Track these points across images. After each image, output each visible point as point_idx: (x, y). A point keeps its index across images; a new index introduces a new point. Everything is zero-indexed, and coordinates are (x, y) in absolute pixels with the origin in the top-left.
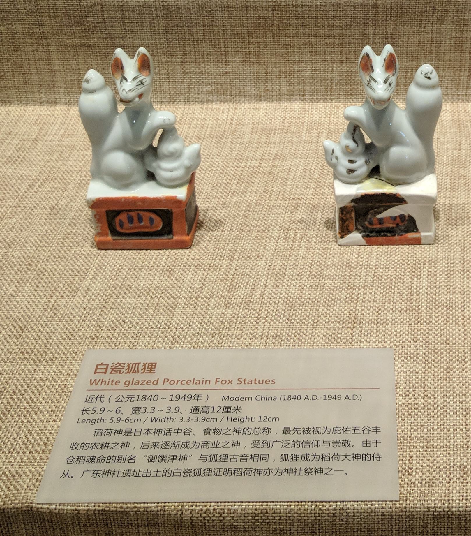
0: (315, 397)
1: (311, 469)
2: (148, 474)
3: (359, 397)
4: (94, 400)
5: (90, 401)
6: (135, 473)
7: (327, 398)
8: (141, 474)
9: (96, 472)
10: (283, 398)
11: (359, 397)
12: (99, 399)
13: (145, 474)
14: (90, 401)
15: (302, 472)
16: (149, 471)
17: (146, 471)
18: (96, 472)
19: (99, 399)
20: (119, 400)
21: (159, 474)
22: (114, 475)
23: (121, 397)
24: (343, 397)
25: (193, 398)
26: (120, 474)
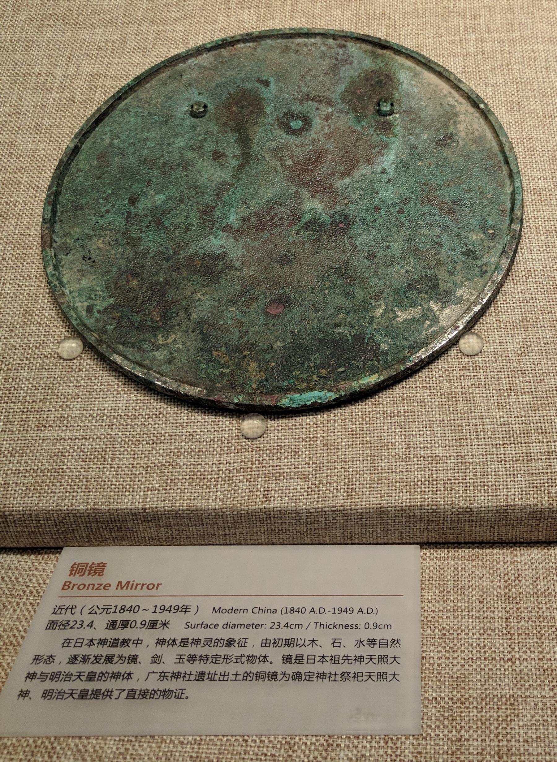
0: (322, 610)
1: (348, 674)
2: (226, 678)
3: (375, 611)
4: (63, 611)
5: (59, 612)
6: (210, 676)
7: (336, 611)
8: (217, 677)
9: (163, 674)
10: (284, 611)
11: (375, 611)
12: (69, 611)
13: (222, 678)
14: (59, 612)
15: (338, 678)
16: (227, 674)
17: (223, 674)
18: (163, 674)
19: (69, 611)
20: (94, 612)
21: (239, 677)
22: (185, 679)
23: (95, 608)
24: (356, 611)
25: (180, 609)
26: (192, 677)
